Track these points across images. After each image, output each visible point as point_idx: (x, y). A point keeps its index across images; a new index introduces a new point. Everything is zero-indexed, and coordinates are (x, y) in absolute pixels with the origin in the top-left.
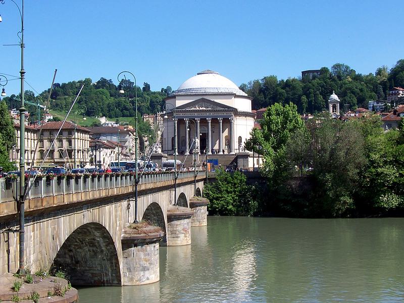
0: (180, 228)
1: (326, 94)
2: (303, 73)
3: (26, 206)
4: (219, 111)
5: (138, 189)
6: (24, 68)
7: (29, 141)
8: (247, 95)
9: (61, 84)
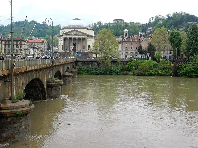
1: (123, 29)
3: (67, 62)
4: (81, 35)
5: (53, 65)
6: (12, 15)
7: (4, 45)
9: (15, 22)
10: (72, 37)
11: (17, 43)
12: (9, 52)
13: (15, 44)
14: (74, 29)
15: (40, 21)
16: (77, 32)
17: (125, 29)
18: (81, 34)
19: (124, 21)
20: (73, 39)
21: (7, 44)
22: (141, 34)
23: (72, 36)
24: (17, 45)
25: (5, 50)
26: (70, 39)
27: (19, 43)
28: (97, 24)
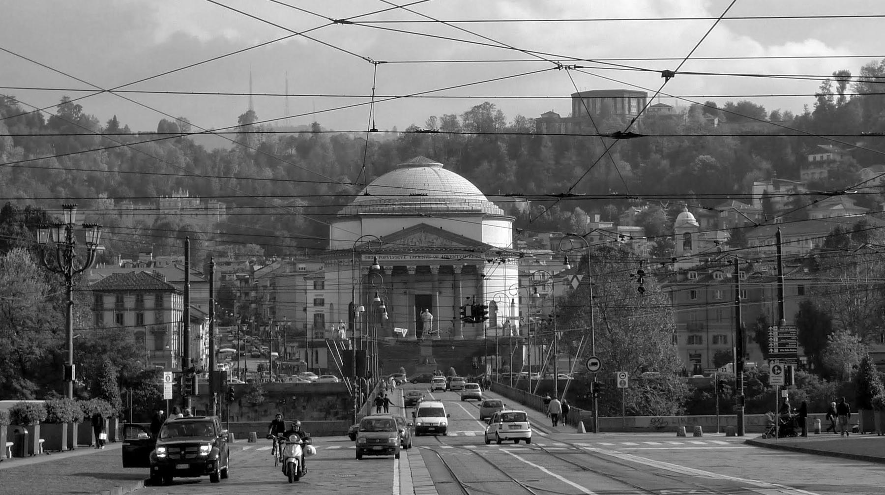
10: (410, 261)
13: (112, 306)
16: (432, 237)
18: (455, 244)
22: (766, 196)
26: (399, 270)
27: (130, 301)
28: (460, 121)
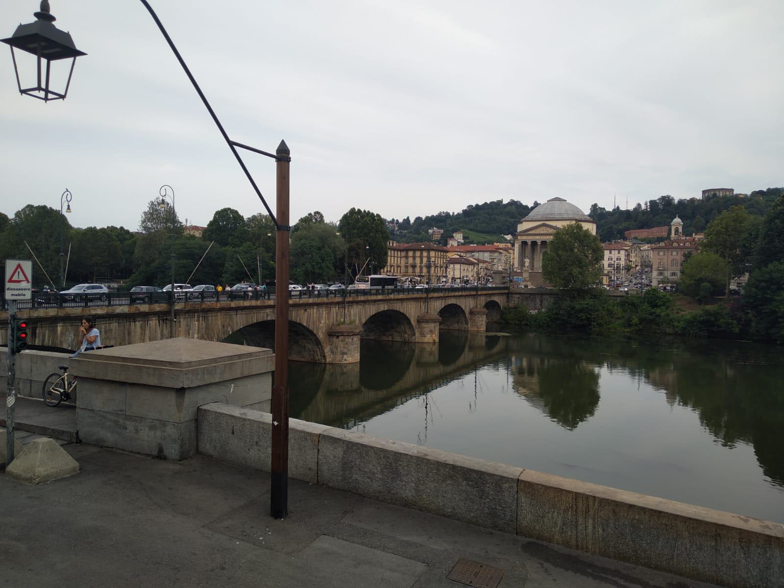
0: (427, 330)
2: (704, 192)
8: (592, 220)
10: (538, 239)
11: (408, 253)
12: (407, 272)
14: (543, 222)
15: (435, 214)
17: (675, 218)
19: (735, 193)
20: (539, 243)
21: (403, 257)
23: (537, 237)
24: (421, 257)
25: (399, 268)
26: (534, 243)
